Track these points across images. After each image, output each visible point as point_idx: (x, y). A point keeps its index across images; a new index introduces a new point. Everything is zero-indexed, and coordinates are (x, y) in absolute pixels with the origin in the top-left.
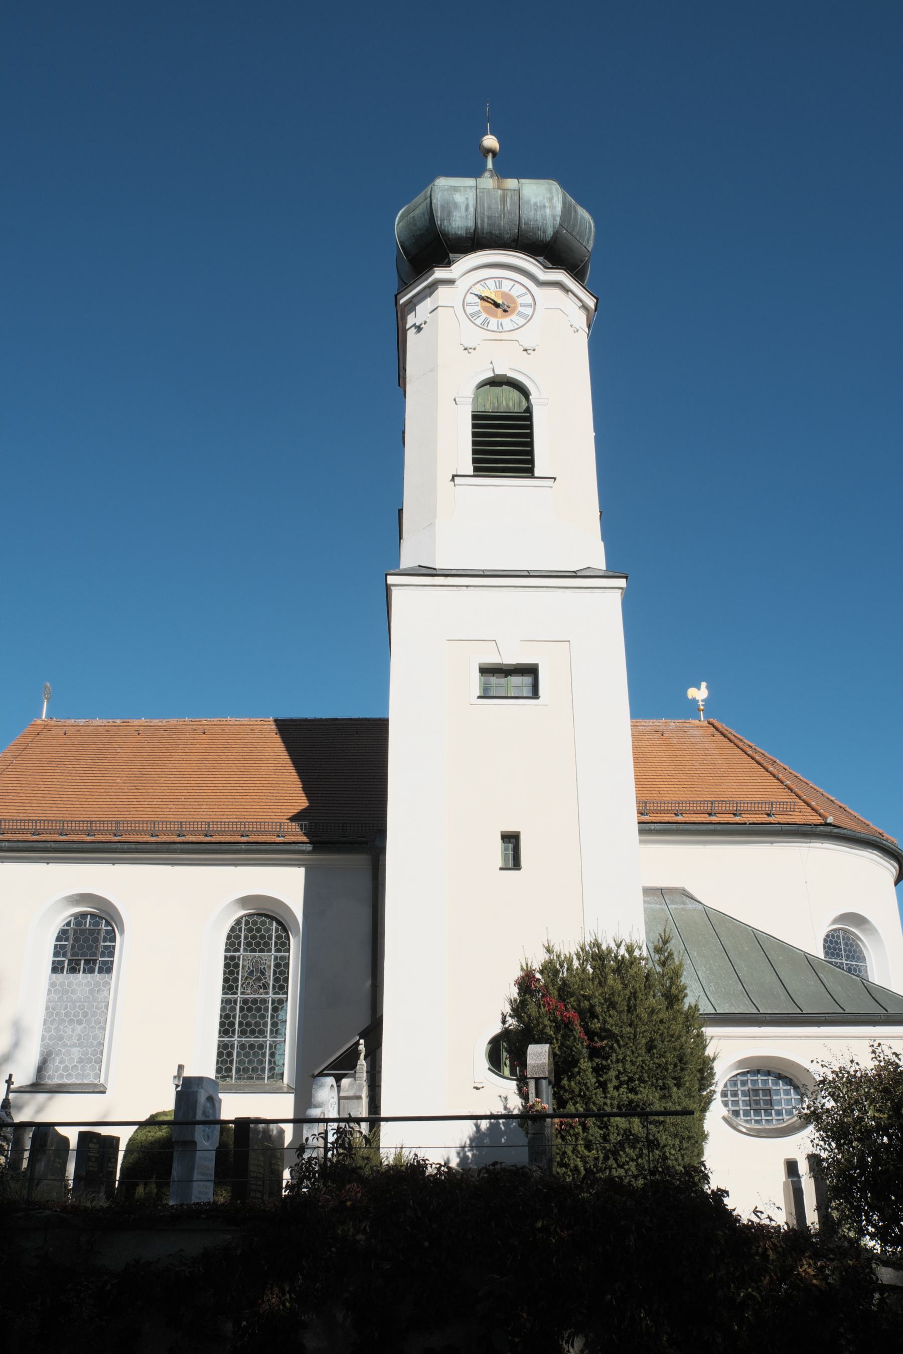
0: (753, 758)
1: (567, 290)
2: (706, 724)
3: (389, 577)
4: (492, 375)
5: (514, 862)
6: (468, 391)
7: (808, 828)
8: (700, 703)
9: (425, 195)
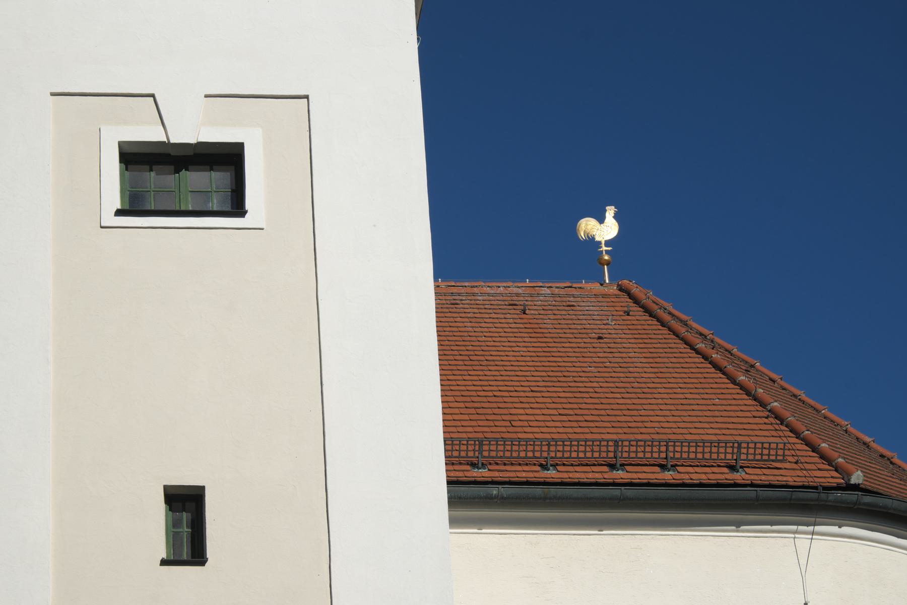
0: (706, 357)
2: (614, 289)
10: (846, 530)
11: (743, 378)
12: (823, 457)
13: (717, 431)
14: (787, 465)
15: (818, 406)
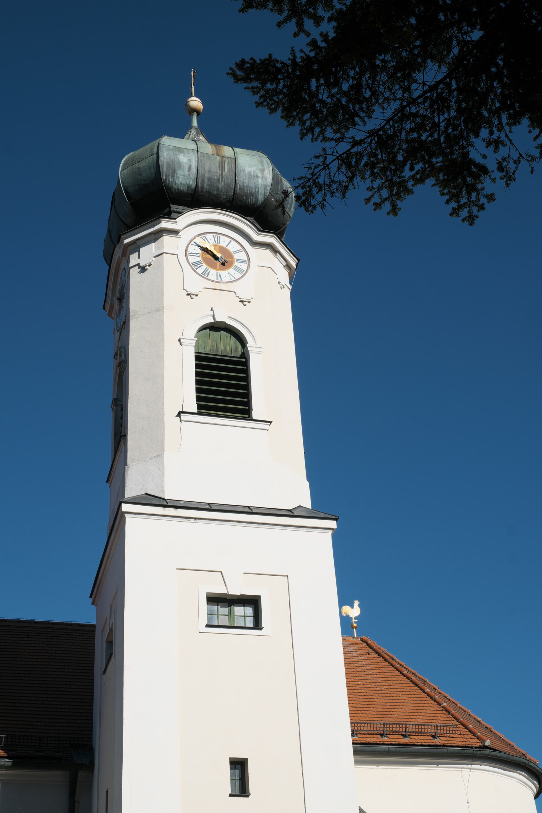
0: (409, 678)
1: (275, 251)
2: (359, 641)
3: (123, 505)
4: (212, 320)
5: (242, 789)
6: (191, 334)
7: (470, 751)
8: (354, 620)
9: (152, 149)
10: (483, 767)
11: (428, 690)
12: (470, 731)
13: (422, 717)
14: (456, 736)
15: (456, 702)
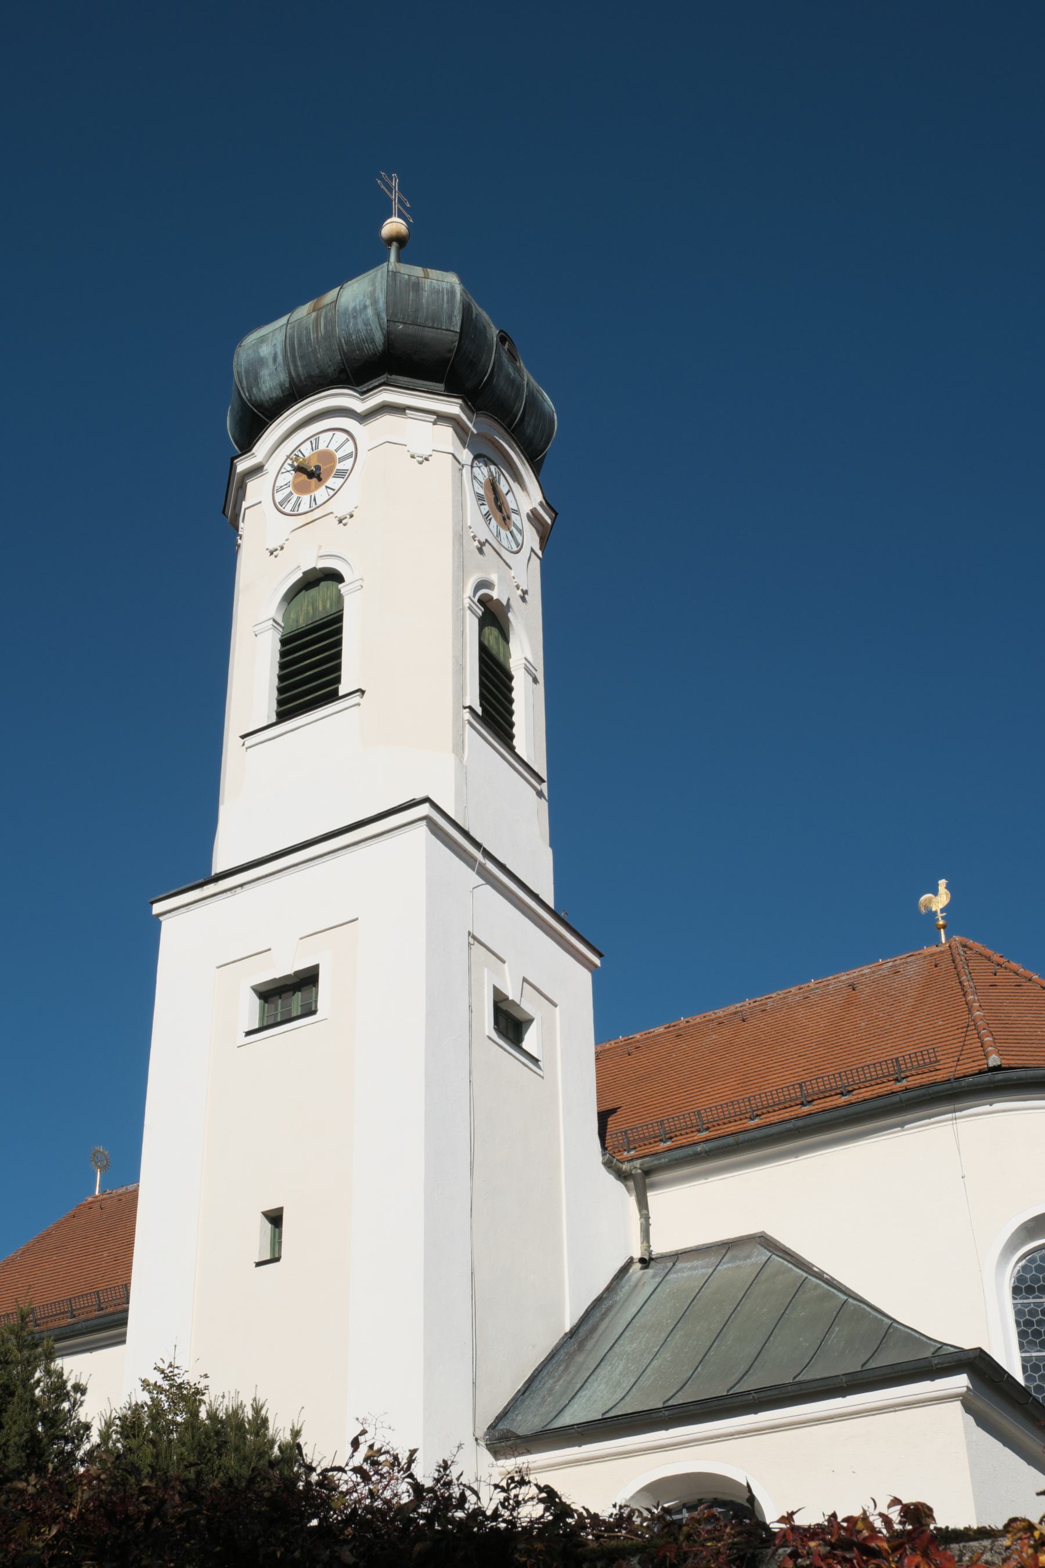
1: (399, 409)
8: (940, 915)
